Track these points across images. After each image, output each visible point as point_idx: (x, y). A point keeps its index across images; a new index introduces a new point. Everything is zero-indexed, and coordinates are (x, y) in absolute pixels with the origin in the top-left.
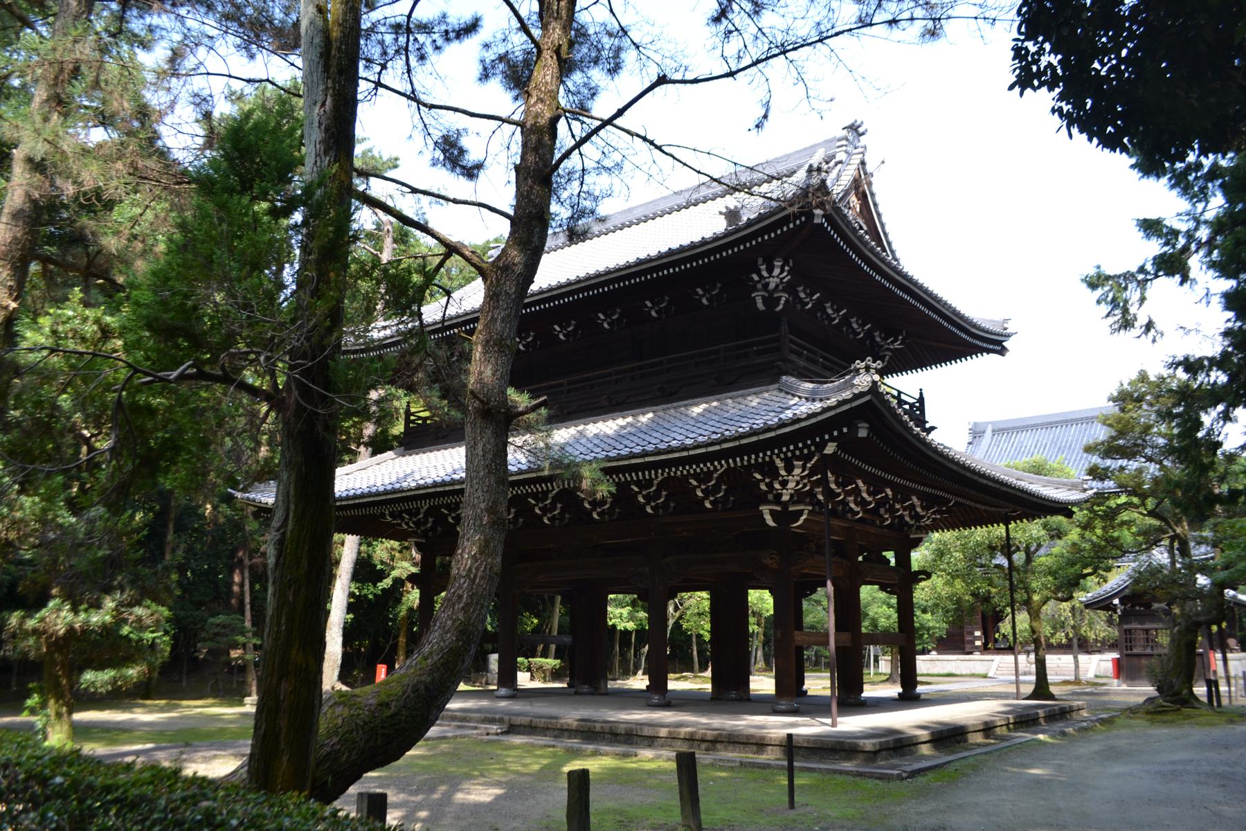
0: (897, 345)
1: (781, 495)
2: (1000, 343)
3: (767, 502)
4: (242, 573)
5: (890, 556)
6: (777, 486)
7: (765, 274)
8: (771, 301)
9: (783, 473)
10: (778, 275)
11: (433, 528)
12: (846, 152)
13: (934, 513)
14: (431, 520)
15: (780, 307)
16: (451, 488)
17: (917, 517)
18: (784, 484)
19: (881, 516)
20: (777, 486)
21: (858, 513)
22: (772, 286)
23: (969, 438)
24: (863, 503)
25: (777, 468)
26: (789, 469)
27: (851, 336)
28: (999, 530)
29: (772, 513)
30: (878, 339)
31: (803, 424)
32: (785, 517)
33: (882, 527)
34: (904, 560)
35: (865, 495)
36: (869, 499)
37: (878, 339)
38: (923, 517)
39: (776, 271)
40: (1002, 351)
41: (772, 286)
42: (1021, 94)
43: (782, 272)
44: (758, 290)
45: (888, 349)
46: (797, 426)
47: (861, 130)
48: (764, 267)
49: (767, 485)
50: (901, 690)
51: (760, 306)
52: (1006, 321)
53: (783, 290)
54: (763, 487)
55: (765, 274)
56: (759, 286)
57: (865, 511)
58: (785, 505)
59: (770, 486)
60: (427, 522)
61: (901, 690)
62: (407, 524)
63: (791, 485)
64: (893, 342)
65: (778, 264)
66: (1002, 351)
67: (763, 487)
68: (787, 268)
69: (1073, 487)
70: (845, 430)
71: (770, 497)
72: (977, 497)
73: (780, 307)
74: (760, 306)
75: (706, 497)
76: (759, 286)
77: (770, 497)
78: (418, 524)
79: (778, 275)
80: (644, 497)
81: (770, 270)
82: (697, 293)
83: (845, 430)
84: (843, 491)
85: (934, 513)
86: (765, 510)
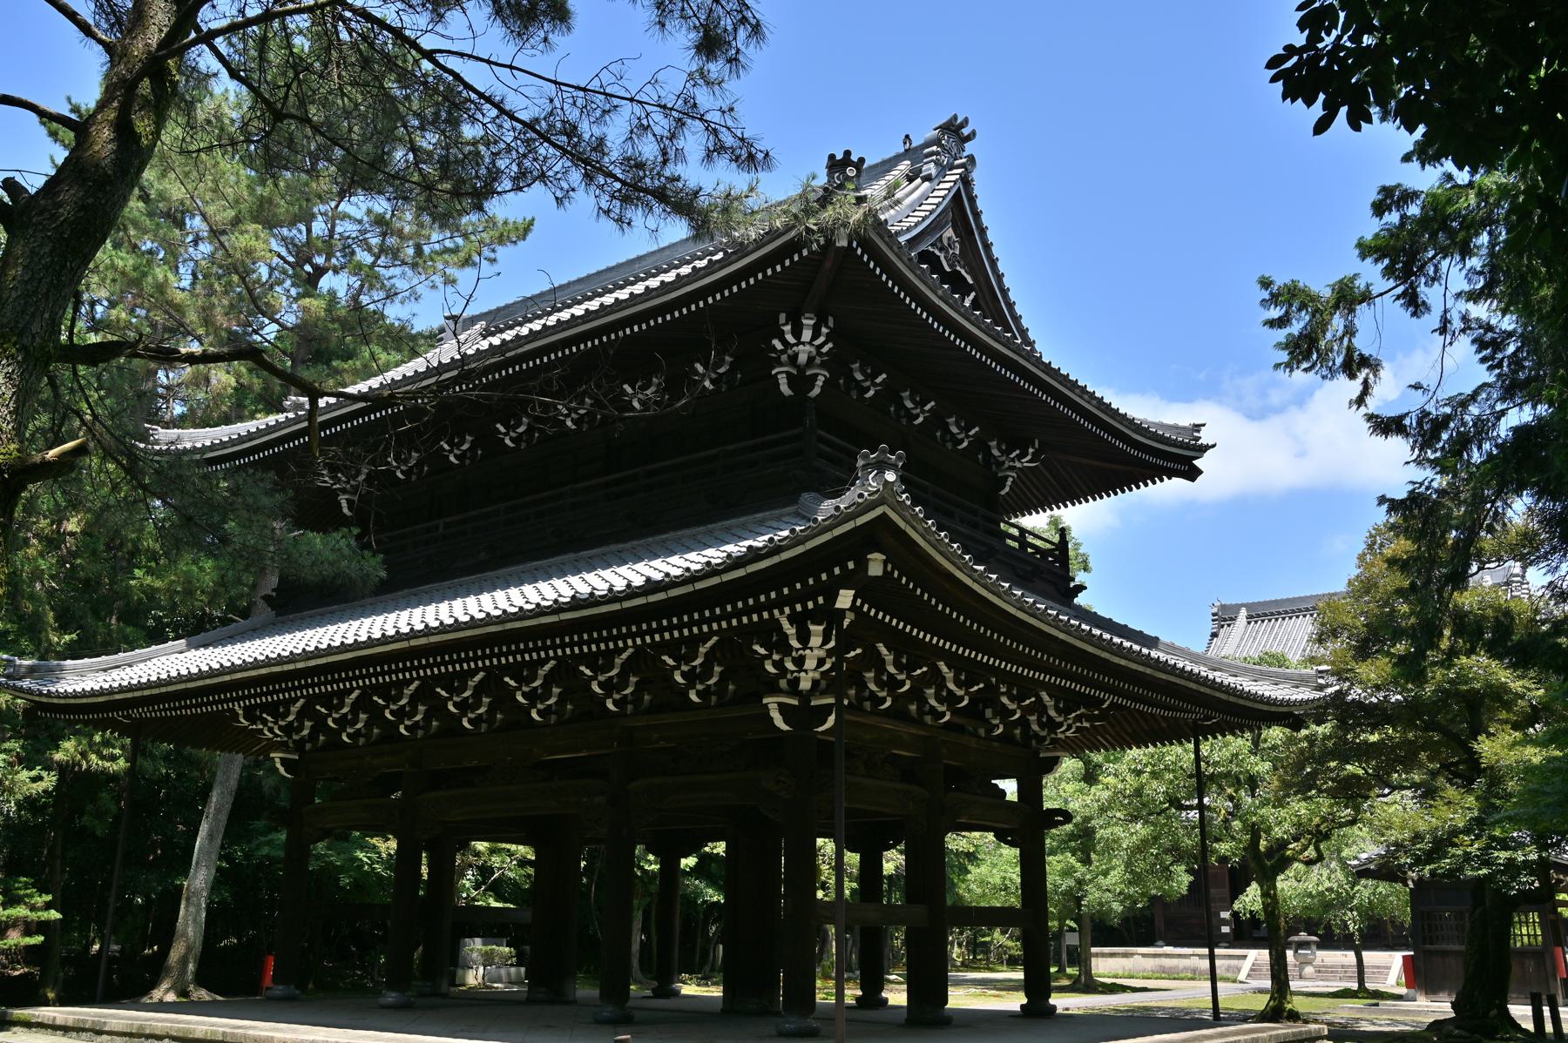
0: (1026, 462)
1: (797, 680)
2: (1188, 461)
3: (776, 691)
4: (258, 848)
5: (1010, 787)
6: (790, 665)
7: (790, 338)
8: (801, 381)
9: (795, 643)
10: (806, 342)
11: (313, 736)
12: (937, 163)
13: (1079, 718)
14: (308, 724)
15: (816, 391)
16: (291, 667)
17: (1052, 726)
18: (800, 662)
19: (987, 721)
20: (790, 665)
21: (943, 714)
22: (803, 358)
23: (1210, 627)
24: (952, 699)
25: (786, 636)
26: (804, 637)
27: (949, 445)
28: (1179, 754)
29: (783, 708)
30: (996, 452)
31: (785, 556)
32: (805, 715)
33: (876, 712)
34: (1030, 791)
35: (1052, 713)
36: (960, 693)
37: (996, 452)
38: (1060, 725)
39: (807, 335)
40: (1192, 474)
41: (803, 358)
42: (1321, 126)
43: (815, 336)
44: (781, 364)
45: (1012, 468)
46: (775, 560)
47: (966, 131)
48: (787, 328)
49: (775, 664)
50: (1025, 1001)
51: (785, 389)
52: (1197, 427)
53: (823, 365)
54: (770, 668)
55: (790, 338)
56: (784, 358)
57: (955, 712)
58: (805, 697)
59: (778, 664)
60: (301, 728)
61: (1025, 1001)
62: (271, 730)
63: (810, 664)
64: (1019, 457)
65: (808, 322)
66: (1192, 474)
67: (770, 668)
68: (824, 330)
69: (1299, 682)
70: (851, 565)
71: (783, 683)
72: (1152, 700)
73: (816, 391)
74: (785, 389)
75: (691, 684)
76: (784, 358)
77: (783, 683)
78: (288, 729)
79: (806, 342)
80: (600, 685)
81: (797, 333)
82: (696, 372)
83: (851, 565)
84: (967, 693)
85: (1079, 718)
86: (771, 702)
